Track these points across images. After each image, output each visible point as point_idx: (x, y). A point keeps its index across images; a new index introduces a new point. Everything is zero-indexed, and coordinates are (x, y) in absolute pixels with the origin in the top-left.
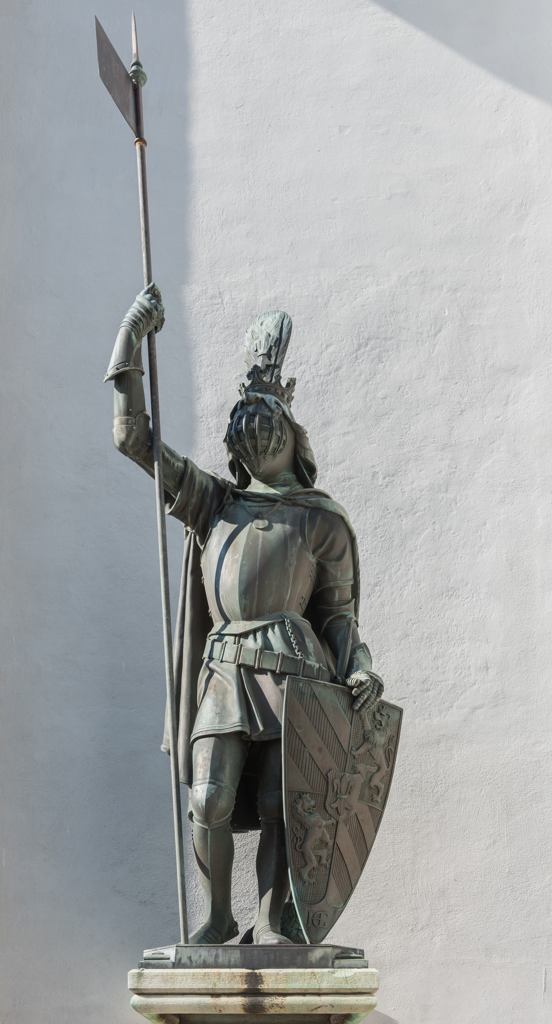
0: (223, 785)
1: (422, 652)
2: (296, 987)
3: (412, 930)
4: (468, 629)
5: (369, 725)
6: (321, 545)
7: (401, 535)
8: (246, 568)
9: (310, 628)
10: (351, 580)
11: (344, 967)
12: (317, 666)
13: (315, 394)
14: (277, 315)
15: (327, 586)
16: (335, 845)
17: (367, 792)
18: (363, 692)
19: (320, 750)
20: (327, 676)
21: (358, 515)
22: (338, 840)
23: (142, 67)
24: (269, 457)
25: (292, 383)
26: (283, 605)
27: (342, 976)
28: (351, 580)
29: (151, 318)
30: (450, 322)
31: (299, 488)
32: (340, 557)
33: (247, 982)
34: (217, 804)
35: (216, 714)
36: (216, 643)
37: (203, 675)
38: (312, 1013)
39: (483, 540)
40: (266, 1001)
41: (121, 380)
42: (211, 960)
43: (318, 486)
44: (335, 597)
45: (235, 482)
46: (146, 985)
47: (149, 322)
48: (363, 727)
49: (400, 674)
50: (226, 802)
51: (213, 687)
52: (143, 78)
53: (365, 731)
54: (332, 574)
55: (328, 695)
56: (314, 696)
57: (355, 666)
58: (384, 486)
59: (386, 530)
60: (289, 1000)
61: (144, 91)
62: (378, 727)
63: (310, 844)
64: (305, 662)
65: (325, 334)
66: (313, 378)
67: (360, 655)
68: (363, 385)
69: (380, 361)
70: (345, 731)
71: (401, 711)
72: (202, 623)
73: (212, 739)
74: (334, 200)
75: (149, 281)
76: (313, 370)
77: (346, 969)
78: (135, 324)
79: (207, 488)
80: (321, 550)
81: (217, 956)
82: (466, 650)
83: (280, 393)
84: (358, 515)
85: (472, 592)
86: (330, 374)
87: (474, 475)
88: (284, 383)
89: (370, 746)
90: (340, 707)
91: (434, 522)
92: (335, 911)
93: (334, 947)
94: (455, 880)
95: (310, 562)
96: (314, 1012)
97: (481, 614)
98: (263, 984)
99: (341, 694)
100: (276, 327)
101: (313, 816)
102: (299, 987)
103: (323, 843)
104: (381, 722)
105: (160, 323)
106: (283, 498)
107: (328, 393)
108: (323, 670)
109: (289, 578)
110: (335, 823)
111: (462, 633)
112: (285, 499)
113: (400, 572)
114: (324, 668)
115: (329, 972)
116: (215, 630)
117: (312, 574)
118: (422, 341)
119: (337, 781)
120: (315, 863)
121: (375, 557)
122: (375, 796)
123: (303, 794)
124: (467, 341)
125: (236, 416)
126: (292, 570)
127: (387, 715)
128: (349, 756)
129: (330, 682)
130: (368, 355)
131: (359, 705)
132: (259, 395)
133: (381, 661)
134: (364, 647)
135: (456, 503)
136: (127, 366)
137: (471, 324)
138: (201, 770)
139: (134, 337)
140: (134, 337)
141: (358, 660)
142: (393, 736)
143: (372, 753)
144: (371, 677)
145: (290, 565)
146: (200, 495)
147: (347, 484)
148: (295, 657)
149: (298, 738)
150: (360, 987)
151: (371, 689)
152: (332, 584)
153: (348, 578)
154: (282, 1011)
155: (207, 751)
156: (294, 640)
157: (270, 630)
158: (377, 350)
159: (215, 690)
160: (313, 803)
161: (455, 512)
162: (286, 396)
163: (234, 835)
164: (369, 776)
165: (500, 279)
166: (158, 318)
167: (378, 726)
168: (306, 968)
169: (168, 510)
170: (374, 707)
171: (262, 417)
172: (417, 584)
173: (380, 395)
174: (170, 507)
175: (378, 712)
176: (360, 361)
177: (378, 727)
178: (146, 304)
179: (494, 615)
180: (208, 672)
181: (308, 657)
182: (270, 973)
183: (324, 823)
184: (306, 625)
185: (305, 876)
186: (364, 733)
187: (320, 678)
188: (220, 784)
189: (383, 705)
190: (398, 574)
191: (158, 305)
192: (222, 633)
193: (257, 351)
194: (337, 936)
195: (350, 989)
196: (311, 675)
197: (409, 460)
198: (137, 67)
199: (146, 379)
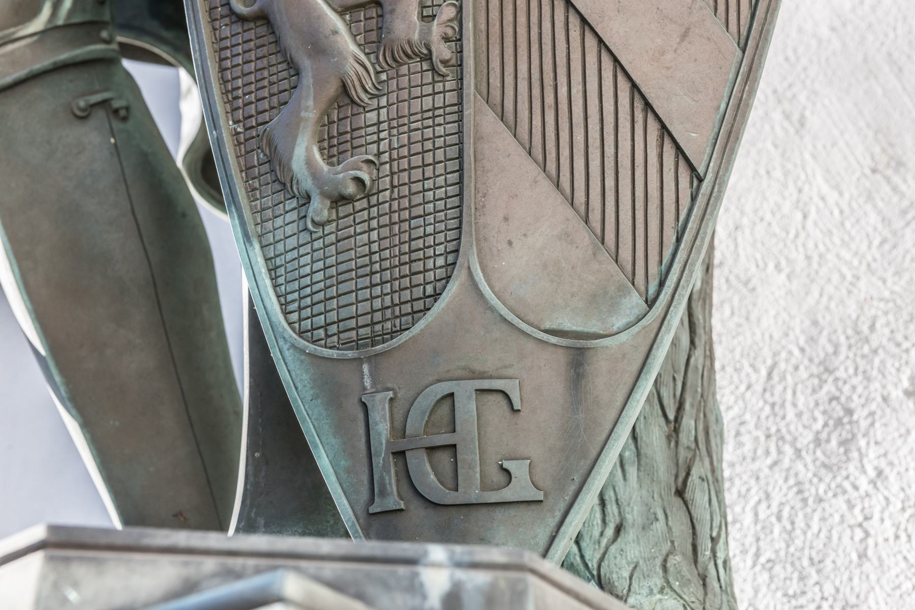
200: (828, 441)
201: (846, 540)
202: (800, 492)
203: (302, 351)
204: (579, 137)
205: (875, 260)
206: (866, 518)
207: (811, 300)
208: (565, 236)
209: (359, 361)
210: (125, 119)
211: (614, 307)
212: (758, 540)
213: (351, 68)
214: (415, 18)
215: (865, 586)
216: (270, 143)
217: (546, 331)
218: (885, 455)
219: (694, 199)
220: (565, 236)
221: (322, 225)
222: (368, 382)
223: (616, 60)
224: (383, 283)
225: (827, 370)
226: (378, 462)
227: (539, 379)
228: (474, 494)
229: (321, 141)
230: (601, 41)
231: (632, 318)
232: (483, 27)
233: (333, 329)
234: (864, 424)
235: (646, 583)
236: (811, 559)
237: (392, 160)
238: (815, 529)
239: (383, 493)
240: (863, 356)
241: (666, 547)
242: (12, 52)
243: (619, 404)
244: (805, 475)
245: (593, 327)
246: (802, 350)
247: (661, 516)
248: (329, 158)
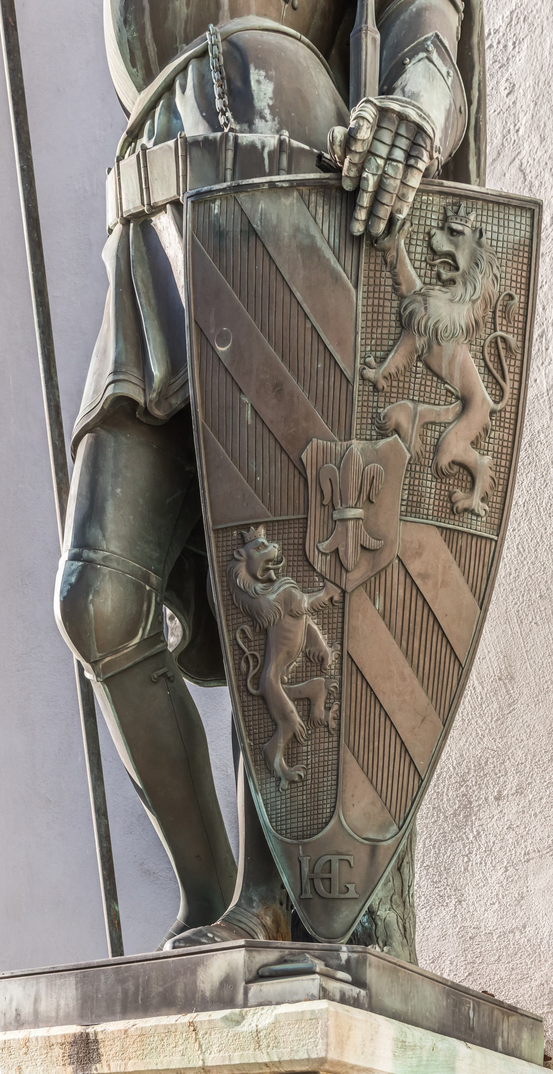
0: (98, 556)
12: (272, 141)
17: (430, 485)
42: (27, 1010)
56: (250, 232)
64: (236, 138)
89: (420, 342)
90: (320, 243)
99: (320, 201)
101: (276, 585)
104: (452, 256)
108: (291, 148)
114: (295, 143)
115: (225, 1019)
122: (459, 494)
123: (247, 527)
143: (434, 364)
183: (306, 601)
188: (92, 555)
200: (459, 815)
201: (460, 861)
202: (444, 836)
203: (277, 838)
204: (381, 764)
205: (493, 728)
206: (470, 853)
207: (461, 743)
208: (373, 803)
209: (298, 845)
210: (172, 681)
211: (387, 830)
212: (424, 856)
213: (298, 728)
214: (323, 709)
215: (465, 882)
216: (265, 753)
217: (364, 839)
218: (482, 825)
219: (419, 788)
220: (373, 803)
221: (285, 790)
222: (301, 853)
223: (397, 731)
224: (307, 816)
225: (464, 780)
226: (304, 881)
227: (360, 857)
228: (336, 895)
229: (285, 755)
230: (392, 723)
231: (393, 834)
232: (348, 714)
233: (289, 831)
234: (476, 809)
235: (384, 907)
236: (445, 867)
237: (312, 768)
238: (448, 854)
239: (306, 892)
240: (480, 777)
241: (392, 892)
242: (126, 653)
243: (386, 865)
244: (447, 829)
245: (380, 837)
246: (454, 768)
247: (391, 880)
248: (287, 763)
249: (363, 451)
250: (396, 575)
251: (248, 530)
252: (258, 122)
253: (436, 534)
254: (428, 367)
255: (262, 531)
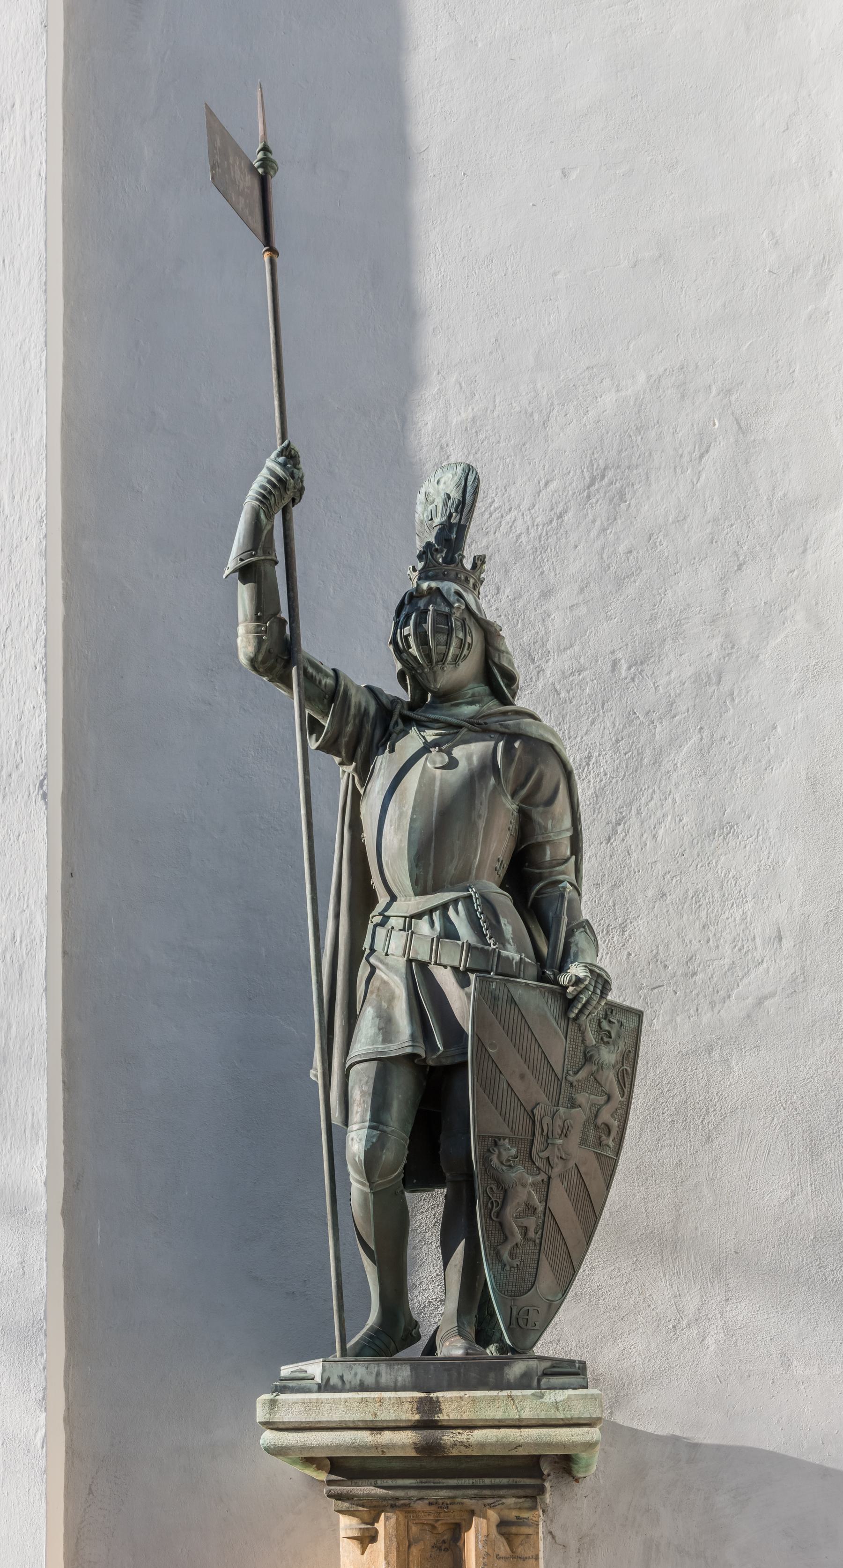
0: (388, 1129)
1: (685, 917)
2: (487, 1417)
3: (674, 1327)
4: (752, 883)
5: (591, 1038)
6: (523, 785)
7: (654, 749)
8: (418, 825)
9: (511, 904)
10: (567, 830)
11: (555, 1388)
12: (517, 957)
13: (530, 552)
14: (460, 469)
15: (533, 841)
16: (547, 1210)
17: (592, 1132)
18: (581, 992)
19: (522, 1076)
20: (533, 971)
21: (593, 723)
22: (551, 1204)
23: (271, 152)
24: (448, 667)
25: (479, 562)
26: (470, 873)
27: (558, 1399)
28: (567, 830)
29: (286, 489)
30: (721, 437)
31: (493, 706)
32: (551, 800)
33: (419, 1410)
34: (381, 1157)
35: (379, 1029)
36: (378, 929)
37: (363, 973)
38: (510, 1453)
39: (772, 751)
40: (446, 1438)
41: (246, 573)
42: (370, 1380)
43: (522, 702)
44: (545, 854)
45: (406, 697)
46: (284, 1416)
47: (284, 493)
48: (583, 1041)
49: (654, 952)
50: (395, 1153)
51: (376, 991)
52: (273, 168)
53: (586, 1047)
54: (539, 824)
55: (533, 999)
56: (512, 1001)
57: (572, 954)
58: (629, 679)
59: (633, 742)
60: (478, 1435)
61: (275, 183)
62: (606, 1039)
63: (510, 1211)
64: (499, 952)
65: (544, 466)
66: (528, 529)
67: (580, 937)
68: (599, 535)
69: (622, 499)
70: (558, 1048)
71: (639, 1015)
72: (363, 899)
73: (375, 1063)
74: (555, 274)
75: (284, 437)
76: (528, 518)
77: (557, 1391)
78: (264, 499)
79: (366, 711)
80: (524, 792)
81: (378, 1374)
82: (749, 913)
83: (463, 578)
84: (593, 723)
85: (757, 827)
86: (551, 522)
87: (758, 656)
88: (468, 565)
89: (594, 1068)
91: (701, 728)
92: (550, 1305)
93: (541, 1358)
94: (736, 1253)
95: (508, 810)
96: (513, 1453)
97: (770, 860)
98: (441, 1413)
100: (458, 485)
101: (515, 1170)
102: (492, 1417)
103: (530, 1209)
104: (609, 1032)
105: (298, 494)
106: (470, 723)
107: (549, 550)
108: (525, 963)
109: (478, 834)
110: (545, 1180)
111: (743, 887)
112: (472, 724)
113: (653, 802)
114: (527, 960)
115: (533, 1395)
116: (379, 908)
117: (511, 826)
118: (682, 467)
119: (547, 1120)
120: (519, 1237)
121: (617, 782)
122: (604, 1137)
123: (499, 1139)
124: (747, 463)
125: (404, 613)
126: (481, 824)
127: (618, 1021)
128: (563, 1083)
129: (538, 981)
130: (605, 493)
131: (576, 1011)
132: (434, 584)
133: (627, 933)
134: (586, 925)
135: (733, 700)
136: (252, 556)
137: (752, 438)
138: (359, 1110)
139: (263, 516)
140: (263, 516)
141: (577, 945)
142: (630, 1051)
143: (599, 1079)
144: (591, 971)
145: (480, 816)
146: (357, 721)
147: (576, 678)
148: (486, 947)
149: (490, 1061)
150: (576, 1416)
151: (592, 988)
152: (540, 839)
153: (564, 828)
154: (469, 1452)
155: (367, 1082)
156: (485, 922)
157: (451, 908)
158: (617, 484)
159: (378, 996)
160: (513, 1151)
161: (731, 712)
162: (472, 581)
163: (407, 1195)
164: (594, 1110)
165: (794, 371)
166: (295, 487)
167: (605, 1038)
168: (502, 1389)
169: (313, 744)
170: (598, 1012)
171: (438, 614)
172: (677, 819)
173: (621, 549)
174: (317, 740)
175: (605, 1019)
176: (594, 500)
177: (606, 1039)
178: (279, 470)
179: (789, 861)
180: (369, 969)
181: (504, 945)
182: (451, 1398)
184: (504, 900)
185: (506, 1256)
186: (585, 1050)
187: (522, 975)
188: (385, 1128)
189: (612, 1008)
190: (650, 805)
191: (295, 471)
192: (386, 914)
193: (432, 519)
194: (550, 1344)
195: (562, 1419)
196: (508, 972)
197: (665, 640)
198: (265, 154)
199: (280, 571)
249: (564, 1113)
250: (575, 1173)
251: (500, 1140)
252: (508, 946)
253: (593, 1154)
254: (595, 1079)
255: (507, 1141)
